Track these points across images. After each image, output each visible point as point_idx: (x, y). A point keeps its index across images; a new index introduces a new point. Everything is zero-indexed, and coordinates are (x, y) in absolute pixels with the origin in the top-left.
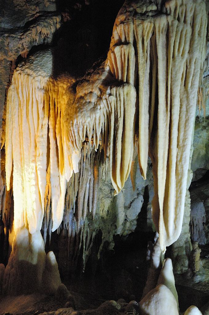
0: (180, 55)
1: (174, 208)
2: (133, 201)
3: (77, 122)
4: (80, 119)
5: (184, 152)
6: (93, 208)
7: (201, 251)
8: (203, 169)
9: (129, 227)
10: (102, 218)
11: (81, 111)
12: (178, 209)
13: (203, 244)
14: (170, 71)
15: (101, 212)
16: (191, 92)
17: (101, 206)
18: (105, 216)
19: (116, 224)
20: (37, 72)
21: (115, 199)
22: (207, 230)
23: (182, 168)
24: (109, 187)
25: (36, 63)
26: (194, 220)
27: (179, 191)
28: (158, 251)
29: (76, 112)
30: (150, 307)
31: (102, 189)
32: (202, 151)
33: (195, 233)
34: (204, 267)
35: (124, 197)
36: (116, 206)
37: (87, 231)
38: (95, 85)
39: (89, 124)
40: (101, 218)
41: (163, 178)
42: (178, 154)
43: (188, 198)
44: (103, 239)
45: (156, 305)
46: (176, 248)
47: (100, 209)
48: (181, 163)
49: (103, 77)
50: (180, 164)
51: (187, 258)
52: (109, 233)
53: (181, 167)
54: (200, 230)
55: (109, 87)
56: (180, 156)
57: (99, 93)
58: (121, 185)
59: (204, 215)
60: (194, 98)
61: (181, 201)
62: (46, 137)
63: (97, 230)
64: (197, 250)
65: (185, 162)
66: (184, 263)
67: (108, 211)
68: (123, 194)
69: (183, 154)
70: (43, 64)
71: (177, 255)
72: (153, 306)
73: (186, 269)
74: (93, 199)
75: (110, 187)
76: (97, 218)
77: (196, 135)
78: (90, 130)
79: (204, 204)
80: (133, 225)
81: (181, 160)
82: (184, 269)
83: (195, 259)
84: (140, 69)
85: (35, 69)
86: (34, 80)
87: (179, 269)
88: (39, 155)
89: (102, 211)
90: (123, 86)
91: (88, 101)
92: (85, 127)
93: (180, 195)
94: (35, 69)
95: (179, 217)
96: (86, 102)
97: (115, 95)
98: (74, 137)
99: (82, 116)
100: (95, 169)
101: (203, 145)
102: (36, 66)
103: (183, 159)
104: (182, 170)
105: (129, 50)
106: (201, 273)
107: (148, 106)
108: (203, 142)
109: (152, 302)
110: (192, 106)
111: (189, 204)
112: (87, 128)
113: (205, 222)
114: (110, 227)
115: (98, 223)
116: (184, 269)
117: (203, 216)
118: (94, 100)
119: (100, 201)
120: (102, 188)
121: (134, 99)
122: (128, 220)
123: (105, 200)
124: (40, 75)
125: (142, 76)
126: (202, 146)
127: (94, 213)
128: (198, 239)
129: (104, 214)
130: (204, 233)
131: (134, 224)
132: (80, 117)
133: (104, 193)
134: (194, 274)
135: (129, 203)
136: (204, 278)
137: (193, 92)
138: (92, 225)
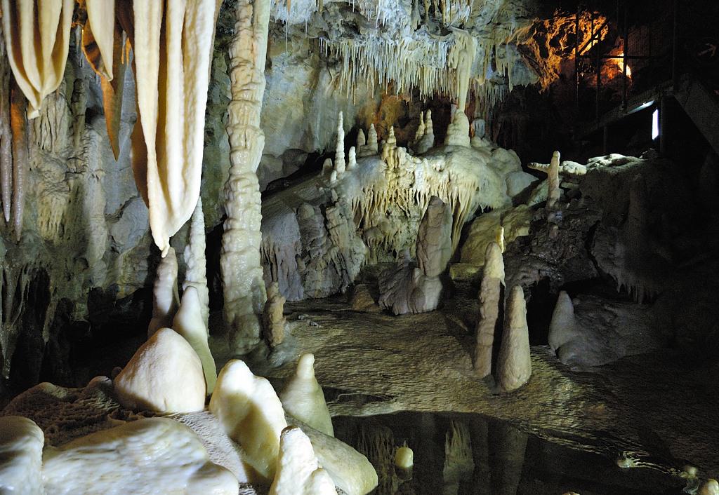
1: (181, 143)
2: (127, 203)
5: (199, 4)
6: (12, 211)
8: (300, 152)
9: (129, 278)
10: (49, 242)
12: (190, 143)
13: (298, 299)
15: (44, 228)
17: (42, 211)
18: (56, 237)
21: (80, 195)
22: (303, 269)
23: (196, 42)
24: (61, 166)
26: (277, 250)
27: (191, 99)
28: (167, 274)
30: (136, 378)
31: (43, 170)
32: (297, 110)
34: (293, 335)
35: (104, 193)
36: (82, 212)
37: (4, 271)
40: (43, 242)
41: (149, 66)
42: (188, 11)
44: (52, 292)
45: (150, 371)
46: (234, 301)
47: (40, 219)
48: (193, 33)
50: (191, 35)
51: (256, 319)
52: (69, 279)
53: (193, 41)
54: (290, 271)
56: (192, 17)
58: (39, 82)
59: (297, 238)
61: (195, 120)
63: (34, 269)
64: (277, 299)
65: (202, 29)
66: (252, 332)
67: (62, 225)
68: (99, 185)
69: (198, 10)
71: (236, 316)
72: (142, 376)
73: (256, 342)
75: (65, 167)
76: (32, 239)
77: (279, 68)
79: (298, 216)
80: (140, 271)
81: (193, 26)
83: (272, 317)
87: (241, 344)
89: (45, 224)
93: (192, 109)
95: (193, 160)
100: (14, 112)
101: (298, 97)
103: (198, 22)
104: (195, 48)
106: (286, 345)
108: (297, 91)
109: (142, 367)
111: (256, 203)
113: (300, 253)
114: (70, 264)
115: (34, 251)
116: (251, 343)
119: (38, 200)
120: (42, 168)
122: (118, 248)
123: (51, 196)
126: (295, 98)
127: (19, 221)
129: (53, 232)
130: (298, 277)
131: (141, 269)
134: (271, 350)
135: (118, 208)
136: (292, 353)
138: (16, 256)
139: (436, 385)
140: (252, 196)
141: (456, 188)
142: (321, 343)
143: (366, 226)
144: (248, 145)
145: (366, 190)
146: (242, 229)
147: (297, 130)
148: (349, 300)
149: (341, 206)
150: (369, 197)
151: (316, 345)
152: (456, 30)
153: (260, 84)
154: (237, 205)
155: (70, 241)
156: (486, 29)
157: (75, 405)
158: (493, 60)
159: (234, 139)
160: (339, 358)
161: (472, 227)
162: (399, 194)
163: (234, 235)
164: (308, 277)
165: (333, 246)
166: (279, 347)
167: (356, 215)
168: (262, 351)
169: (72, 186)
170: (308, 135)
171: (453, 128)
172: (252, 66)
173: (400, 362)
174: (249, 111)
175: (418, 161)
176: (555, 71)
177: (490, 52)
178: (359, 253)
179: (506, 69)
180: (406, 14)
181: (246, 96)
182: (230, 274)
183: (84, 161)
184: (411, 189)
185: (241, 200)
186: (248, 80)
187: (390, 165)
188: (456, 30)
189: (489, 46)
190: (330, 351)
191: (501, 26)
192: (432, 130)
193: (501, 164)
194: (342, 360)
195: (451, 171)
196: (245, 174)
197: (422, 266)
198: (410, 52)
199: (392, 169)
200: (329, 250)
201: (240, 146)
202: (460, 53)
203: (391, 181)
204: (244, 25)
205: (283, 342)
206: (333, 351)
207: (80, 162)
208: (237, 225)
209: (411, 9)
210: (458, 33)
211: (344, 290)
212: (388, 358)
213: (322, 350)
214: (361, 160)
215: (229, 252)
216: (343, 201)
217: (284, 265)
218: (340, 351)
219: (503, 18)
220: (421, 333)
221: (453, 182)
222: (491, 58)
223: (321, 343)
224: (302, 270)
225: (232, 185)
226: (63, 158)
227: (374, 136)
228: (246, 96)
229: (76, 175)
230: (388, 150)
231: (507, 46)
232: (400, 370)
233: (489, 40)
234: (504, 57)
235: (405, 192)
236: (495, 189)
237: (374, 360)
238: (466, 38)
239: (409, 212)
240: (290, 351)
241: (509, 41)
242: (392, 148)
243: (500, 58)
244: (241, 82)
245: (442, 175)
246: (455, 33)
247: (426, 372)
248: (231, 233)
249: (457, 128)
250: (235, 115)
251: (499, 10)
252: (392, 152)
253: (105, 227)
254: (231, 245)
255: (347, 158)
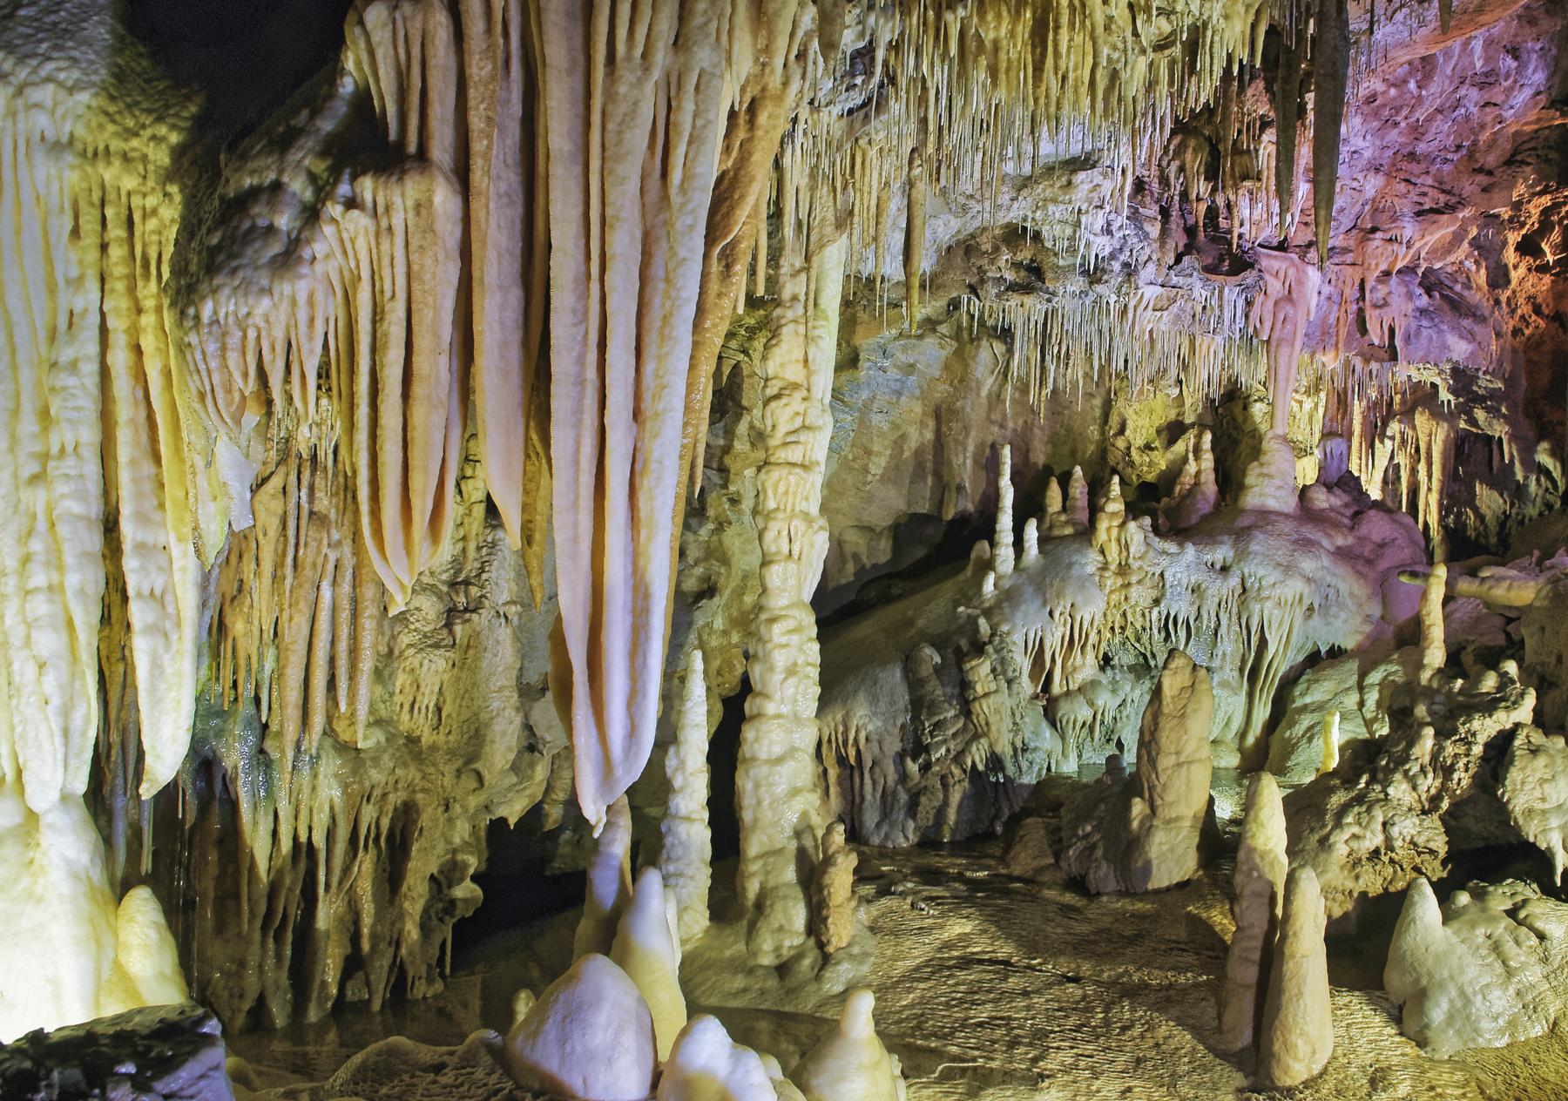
0: (638, 51)
3: (215, 312)
4: (229, 298)
7: (855, 863)
11: (234, 264)
14: (596, 118)
15: (405, 716)
16: (683, 205)
19: (478, 766)
20: (34, 62)
24: (440, 598)
25: (29, 18)
29: (211, 269)
33: (868, 797)
38: (294, 156)
39: (267, 321)
40: (401, 741)
43: (805, 638)
47: (398, 699)
49: (327, 125)
52: (447, 809)
55: (348, 170)
57: (308, 195)
60: (691, 228)
62: (90, 369)
64: (840, 859)
66: (790, 920)
68: (509, 631)
70: (63, 26)
71: (762, 888)
73: (798, 941)
74: (354, 651)
75: (447, 598)
78: (273, 349)
82: (787, 943)
84: (472, 103)
85: (25, 50)
86: (20, 102)
88: (63, 450)
89: (407, 707)
90: (403, 172)
91: (262, 223)
92: (252, 334)
94: (25, 50)
96: (253, 227)
97: (369, 205)
98: (204, 374)
99: (236, 289)
102: (30, 31)
105: (425, 22)
106: (856, 950)
107: (518, 251)
110: (684, 260)
112: (258, 338)
116: (787, 943)
117: (899, 723)
118: (284, 221)
121: (449, 227)
124: (49, 80)
125: (481, 131)
128: (878, 825)
130: (903, 797)
132: (226, 291)
133: (418, 625)
137: (690, 206)
139: (1138, 1061)
140: (801, 650)
141: (1258, 607)
142: (927, 948)
143: (1057, 688)
144: (796, 553)
145: (1057, 615)
146: (779, 716)
147: (919, 473)
148: (1007, 851)
149: (997, 651)
150: (1061, 629)
151: (916, 953)
152: (1268, 256)
153: (819, 428)
154: (771, 669)
155: (451, 738)
156: (1344, 244)
157: (443, 1080)
158: (1361, 311)
159: (769, 536)
160: (957, 984)
161: (1297, 691)
162: (1130, 618)
163: (764, 728)
164: (923, 799)
165: (976, 737)
166: (841, 954)
167: (1034, 665)
168: (807, 962)
169: (458, 636)
170: (944, 487)
171: (1257, 471)
172: (804, 393)
173: (1078, 1002)
174: (797, 485)
175: (1171, 547)
176: (1537, 310)
177: (1351, 293)
178: (1035, 749)
179: (1392, 331)
180: (1146, 236)
181: (795, 454)
182: (754, 802)
183: (482, 587)
184: (1155, 611)
185: (780, 659)
186: (798, 422)
187: (1110, 559)
188: (1268, 256)
189: (1349, 281)
190: (942, 968)
191: (1379, 235)
192: (1212, 477)
193: (1371, 546)
194: (962, 988)
195: (1246, 571)
196: (788, 607)
197: (1147, 795)
198: (1159, 314)
199: (1113, 567)
200: (968, 744)
201: (778, 552)
202: (1276, 303)
203: (1112, 592)
204: (790, 314)
205: (849, 945)
206: (949, 968)
207: (474, 591)
208: (770, 708)
209: (1158, 226)
210: (1272, 262)
211: (999, 829)
212: (1056, 991)
213: (927, 964)
214: (1049, 547)
215: (753, 759)
216: (1002, 641)
217: (877, 769)
218: (962, 969)
219: (1385, 216)
220: (1132, 941)
221: (1252, 594)
222: (1355, 307)
223: (927, 948)
224: (911, 784)
225: (763, 629)
226: (444, 582)
227: (1079, 488)
228: (795, 454)
229: (467, 615)
230: (1106, 528)
231: (1394, 279)
232: (1073, 1020)
233: (1350, 269)
234: (1385, 304)
235: (1143, 615)
236: (1354, 608)
237: (1026, 994)
238: (1292, 272)
239: (1154, 656)
240: (862, 963)
241: (1399, 265)
242: (1116, 523)
243: (1375, 306)
244: (783, 429)
245: (1225, 579)
246: (1264, 263)
247: (1124, 1029)
248: (756, 723)
249: (1265, 471)
250: (770, 493)
251: (1374, 200)
252: (1115, 532)
253: (518, 710)
254: (756, 746)
255: (1018, 544)
